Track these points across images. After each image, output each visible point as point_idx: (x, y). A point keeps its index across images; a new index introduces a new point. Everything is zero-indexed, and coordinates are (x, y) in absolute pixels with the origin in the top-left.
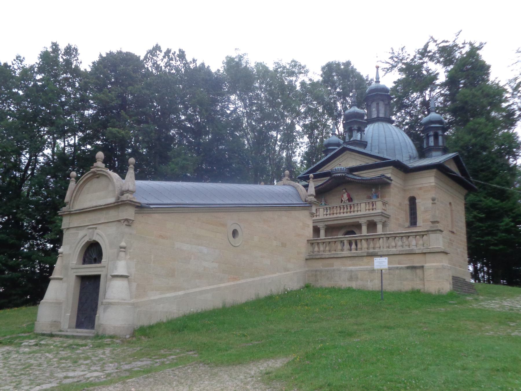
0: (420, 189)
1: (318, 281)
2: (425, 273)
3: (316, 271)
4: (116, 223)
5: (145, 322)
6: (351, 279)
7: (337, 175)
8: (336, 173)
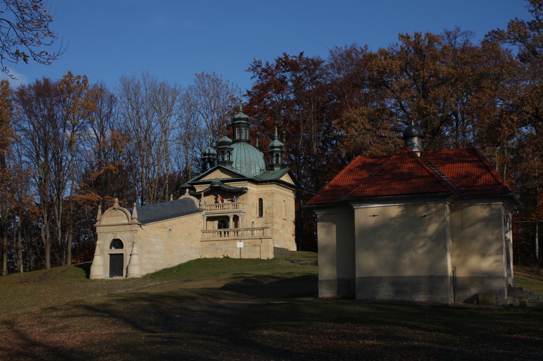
0: (265, 194)
8: (215, 184)
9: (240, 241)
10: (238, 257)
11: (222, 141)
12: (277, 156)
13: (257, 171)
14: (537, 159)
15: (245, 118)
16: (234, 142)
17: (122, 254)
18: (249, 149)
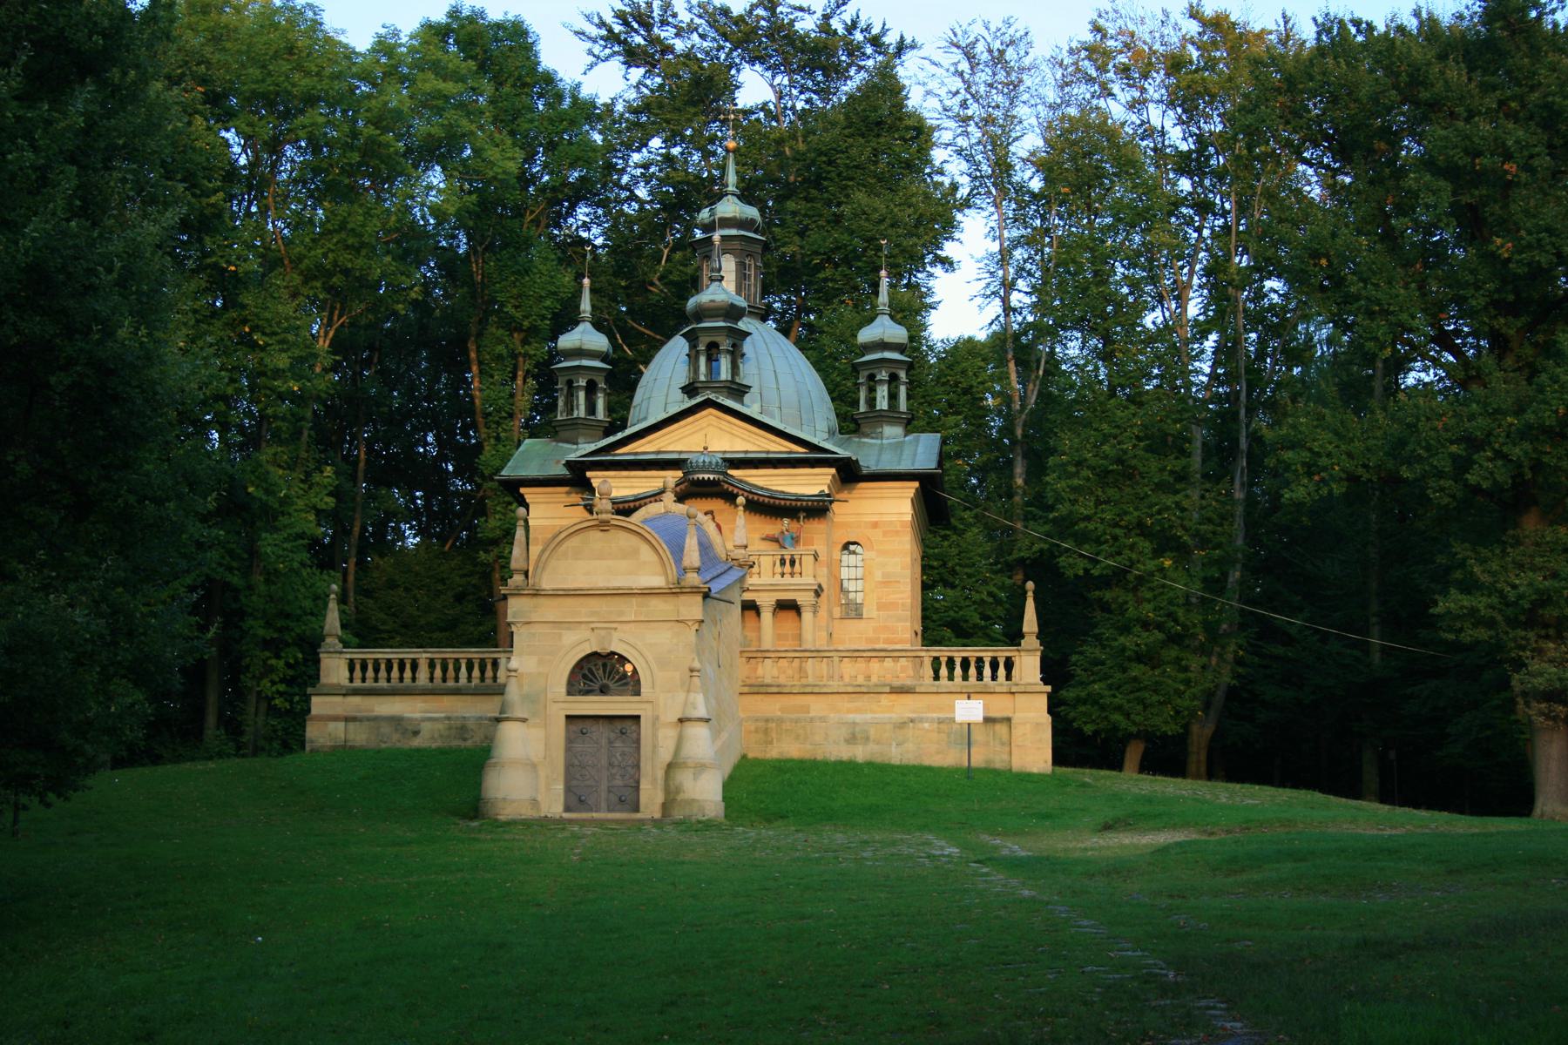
0: (875, 525)
1: (771, 743)
3: (767, 721)
4: (670, 624)
6: (852, 739)
7: (701, 476)
8: (699, 472)
11: (712, 301)
14: (1200, 413)
17: (637, 718)
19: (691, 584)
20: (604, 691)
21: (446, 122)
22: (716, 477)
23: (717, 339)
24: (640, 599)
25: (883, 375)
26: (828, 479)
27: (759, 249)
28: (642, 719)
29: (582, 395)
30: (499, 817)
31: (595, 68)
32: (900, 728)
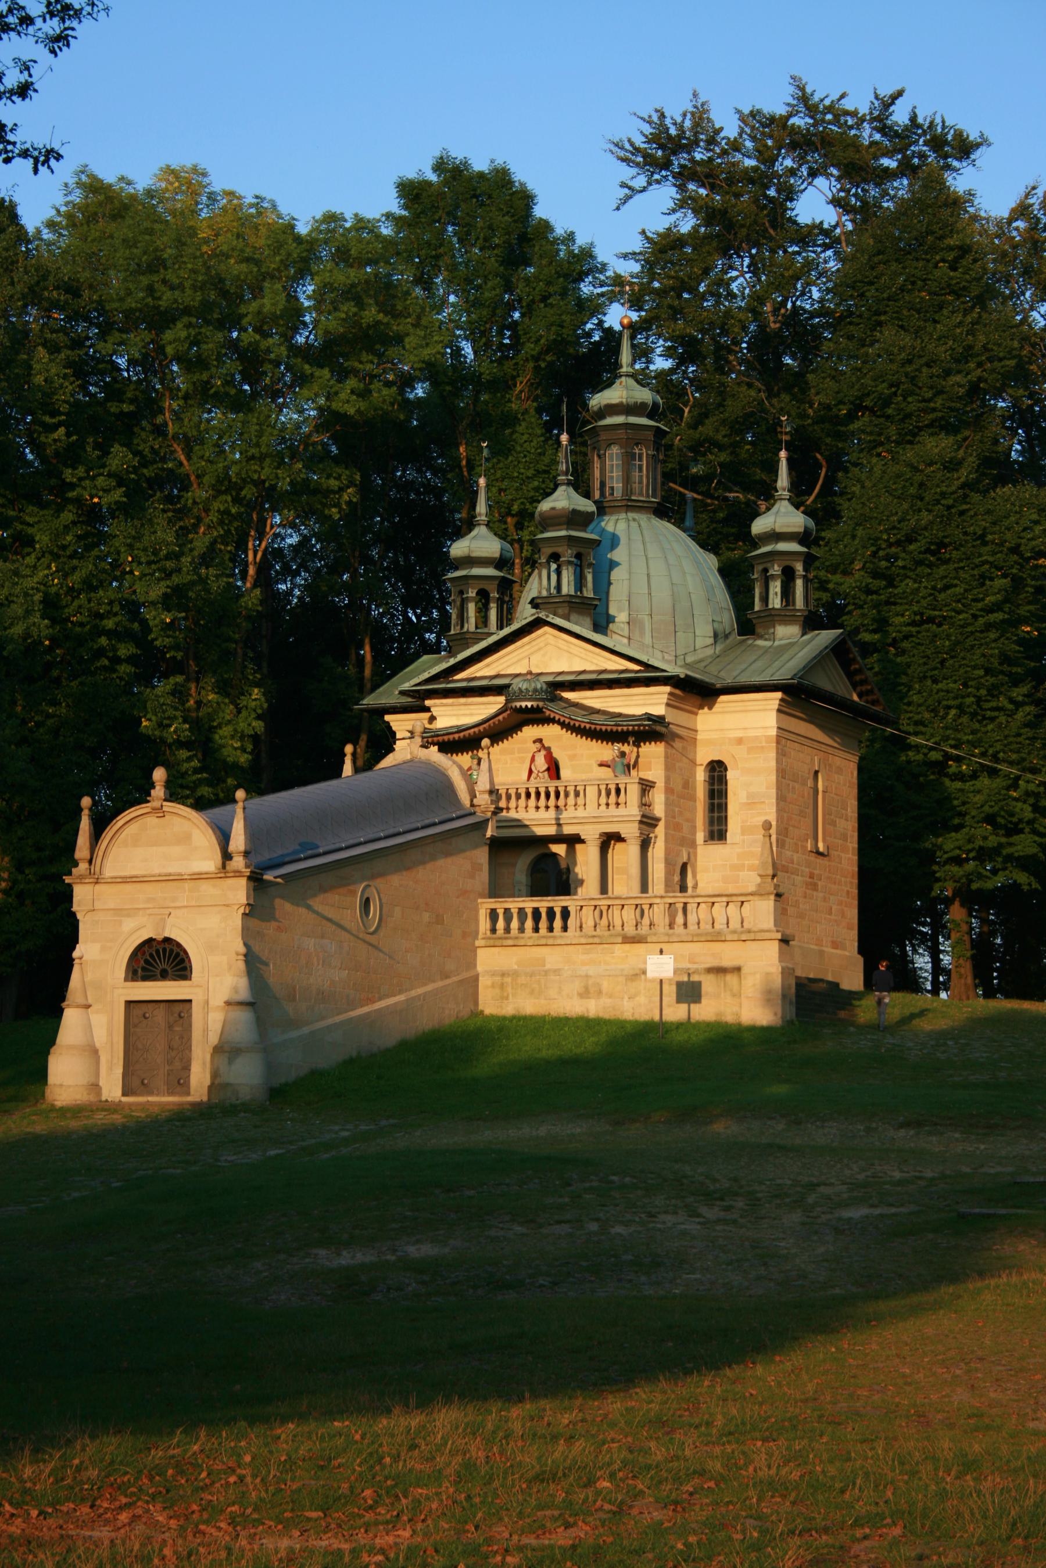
0: (740, 741)
1: (507, 998)
2: (743, 982)
3: (503, 975)
5: (722, 975)
9: (661, 952)
10: (692, 1006)
11: (553, 509)
12: (788, 575)
13: (700, 643)
15: (643, 405)
16: (602, 509)
18: (653, 551)
19: (236, 868)
20: (164, 976)
21: (343, 316)
22: (535, 704)
23: (559, 550)
24: (192, 884)
25: (776, 569)
26: (665, 698)
27: (650, 435)
28: (194, 1003)
29: (471, 607)
30: (56, 1103)
31: (631, 201)
32: (632, 980)
